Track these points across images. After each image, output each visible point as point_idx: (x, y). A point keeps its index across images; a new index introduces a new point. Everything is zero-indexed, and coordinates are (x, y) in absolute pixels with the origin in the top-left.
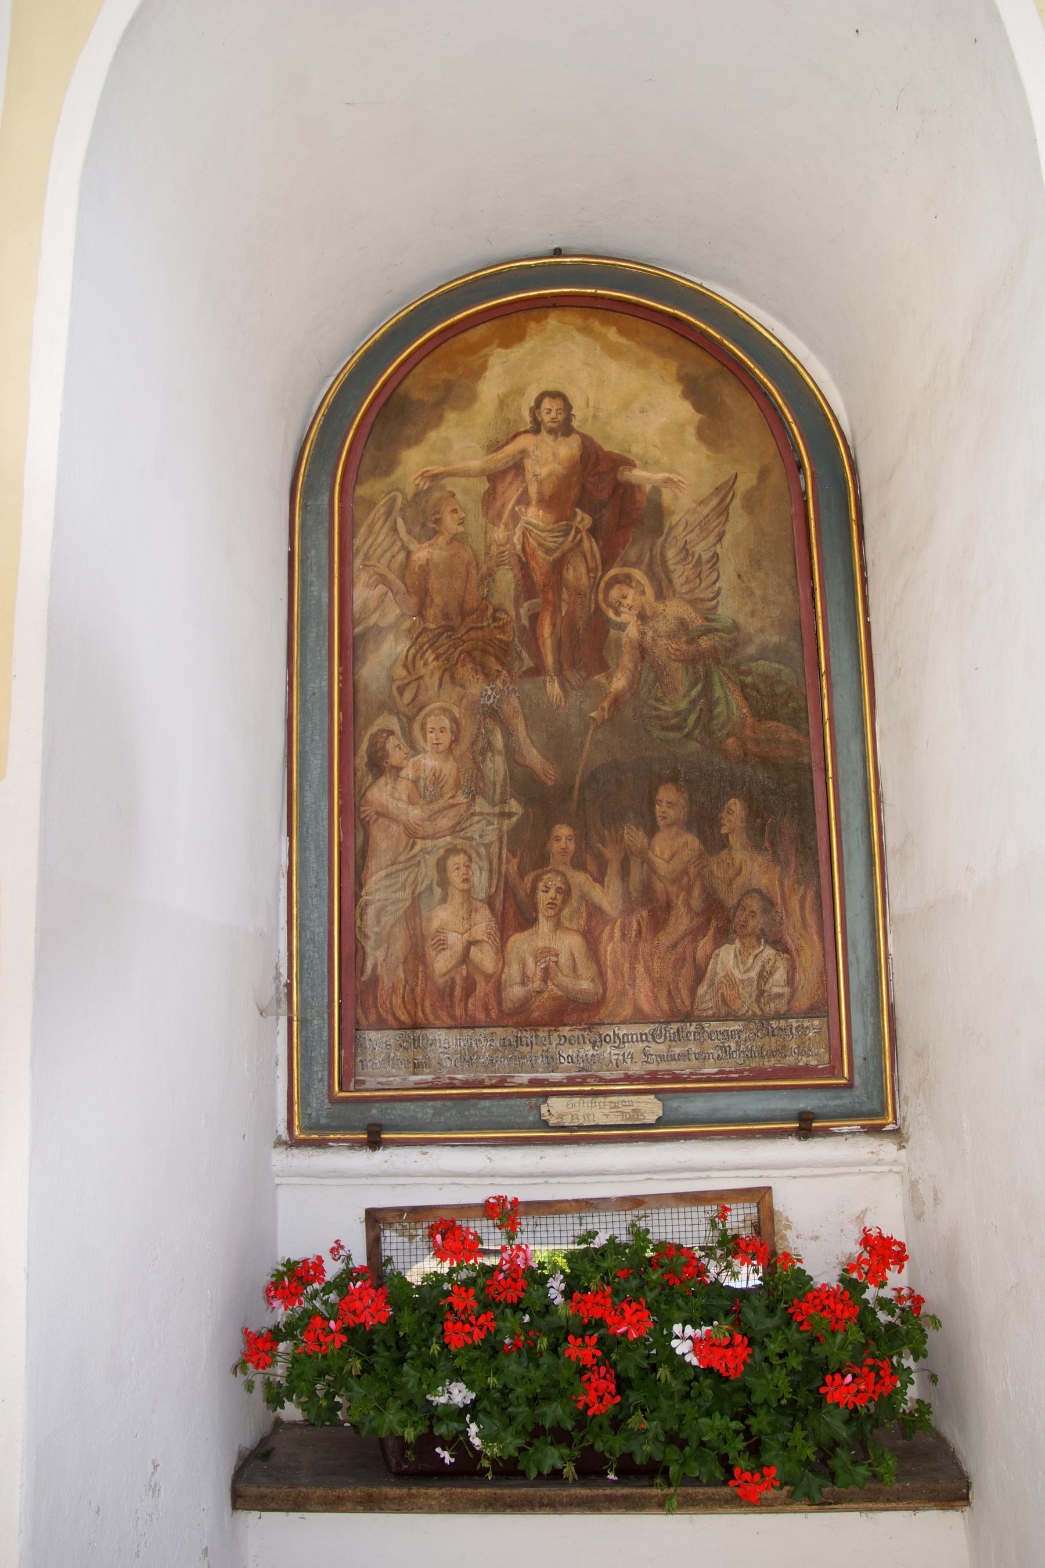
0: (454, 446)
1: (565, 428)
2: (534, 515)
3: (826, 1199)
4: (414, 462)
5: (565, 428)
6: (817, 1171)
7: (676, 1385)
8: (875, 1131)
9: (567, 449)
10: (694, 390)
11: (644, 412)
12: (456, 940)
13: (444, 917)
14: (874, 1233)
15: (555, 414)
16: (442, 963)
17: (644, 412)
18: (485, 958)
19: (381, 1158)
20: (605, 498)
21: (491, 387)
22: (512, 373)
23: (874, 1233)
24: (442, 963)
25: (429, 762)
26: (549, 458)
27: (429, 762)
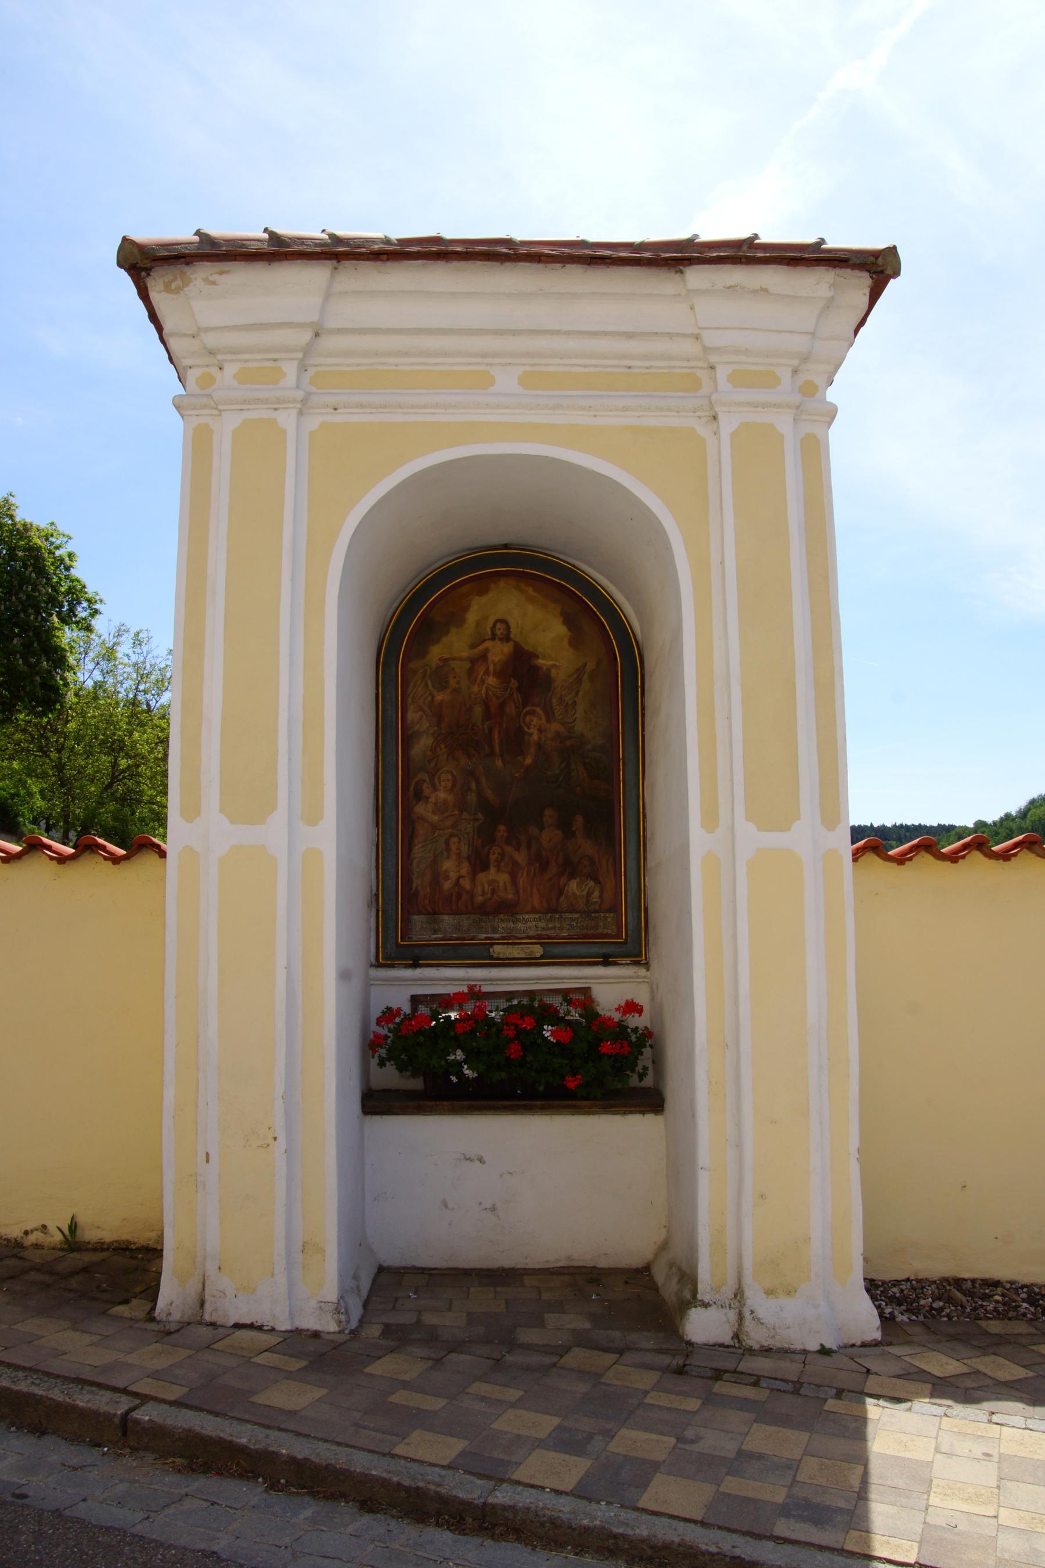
0: (454, 645)
1: (507, 638)
2: (491, 680)
3: (610, 987)
4: (436, 652)
5: (507, 638)
8: (637, 963)
9: (507, 648)
10: (569, 621)
11: (545, 632)
12: (453, 875)
13: (448, 865)
15: (502, 631)
16: (447, 885)
17: (545, 632)
18: (466, 884)
19: (418, 972)
20: (524, 671)
21: (472, 617)
24: (447, 885)
25: (442, 795)
26: (498, 652)
27: (442, 795)
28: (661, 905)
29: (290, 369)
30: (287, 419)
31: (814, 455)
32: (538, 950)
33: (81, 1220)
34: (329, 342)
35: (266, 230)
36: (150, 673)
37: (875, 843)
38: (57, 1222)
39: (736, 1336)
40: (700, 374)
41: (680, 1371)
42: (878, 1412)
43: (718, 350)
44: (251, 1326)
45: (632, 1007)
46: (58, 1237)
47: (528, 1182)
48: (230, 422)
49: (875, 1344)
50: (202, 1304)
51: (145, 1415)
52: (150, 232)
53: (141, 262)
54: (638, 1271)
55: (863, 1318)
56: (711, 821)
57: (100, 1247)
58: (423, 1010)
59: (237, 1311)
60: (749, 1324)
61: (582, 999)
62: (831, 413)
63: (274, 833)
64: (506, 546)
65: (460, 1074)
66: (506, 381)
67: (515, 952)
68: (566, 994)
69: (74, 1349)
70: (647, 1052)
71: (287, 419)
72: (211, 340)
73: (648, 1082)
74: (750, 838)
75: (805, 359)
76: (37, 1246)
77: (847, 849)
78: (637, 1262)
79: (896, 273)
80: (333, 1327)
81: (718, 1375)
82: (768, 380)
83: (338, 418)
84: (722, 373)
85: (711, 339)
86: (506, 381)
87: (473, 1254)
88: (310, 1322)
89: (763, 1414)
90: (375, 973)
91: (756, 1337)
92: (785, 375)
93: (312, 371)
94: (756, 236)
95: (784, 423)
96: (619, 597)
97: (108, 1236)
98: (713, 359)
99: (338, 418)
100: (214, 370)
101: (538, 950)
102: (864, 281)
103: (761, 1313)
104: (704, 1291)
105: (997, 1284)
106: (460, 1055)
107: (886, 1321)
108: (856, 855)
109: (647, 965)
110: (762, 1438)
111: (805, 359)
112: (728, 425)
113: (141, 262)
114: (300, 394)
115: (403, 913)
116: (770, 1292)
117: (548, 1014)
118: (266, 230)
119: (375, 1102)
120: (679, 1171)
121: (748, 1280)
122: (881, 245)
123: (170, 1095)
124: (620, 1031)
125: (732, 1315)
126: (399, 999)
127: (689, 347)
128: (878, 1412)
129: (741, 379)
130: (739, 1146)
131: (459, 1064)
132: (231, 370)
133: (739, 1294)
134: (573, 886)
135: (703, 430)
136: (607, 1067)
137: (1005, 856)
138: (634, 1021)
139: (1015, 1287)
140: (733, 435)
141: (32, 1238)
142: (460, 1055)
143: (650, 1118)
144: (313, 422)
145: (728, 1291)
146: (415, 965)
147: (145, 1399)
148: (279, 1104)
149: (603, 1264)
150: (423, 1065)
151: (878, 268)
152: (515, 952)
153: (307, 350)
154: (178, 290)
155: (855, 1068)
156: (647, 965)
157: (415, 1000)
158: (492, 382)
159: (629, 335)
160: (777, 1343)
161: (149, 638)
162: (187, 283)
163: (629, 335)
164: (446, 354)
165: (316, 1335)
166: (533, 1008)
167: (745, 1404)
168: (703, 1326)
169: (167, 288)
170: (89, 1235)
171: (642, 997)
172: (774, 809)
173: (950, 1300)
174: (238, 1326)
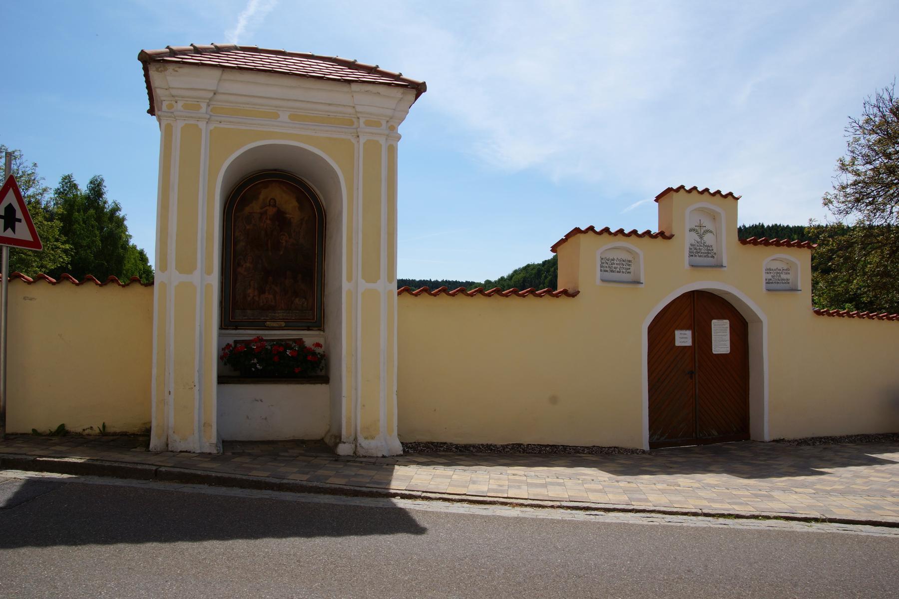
0: (255, 207)
1: (275, 206)
2: (268, 222)
3: (310, 338)
4: (247, 210)
5: (275, 206)
6: (511, 501)
7: (888, 151)
8: (320, 330)
9: (275, 210)
10: (298, 200)
11: (289, 204)
12: (251, 295)
13: (250, 291)
14: (121, 214)
15: (273, 203)
16: (249, 299)
17: (289, 204)
18: (257, 299)
19: (237, 331)
20: (281, 218)
21: (262, 197)
22: (264, 194)
23: (121, 214)
24: (249, 299)
25: (248, 265)
26: (271, 211)
27: (248, 265)
28: (330, 308)
29: (204, 106)
30: (202, 125)
31: (392, 152)
32: (283, 324)
33: (106, 424)
34: (218, 97)
35: (192, 45)
36: (21, 177)
37: (407, 287)
38: (97, 427)
39: (355, 453)
40: (354, 120)
41: (336, 460)
42: (396, 467)
43: (360, 112)
44: (186, 452)
45: (318, 345)
46: (98, 431)
47: (280, 408)
48: (179, 125)
49: (401, 455)
50: (167, 445)
51: (163, 469)
52: (152, 48)
53: (148, 60)
54: (319, 441)
55: (398, 448)
56: (350, 279)
57: (115, 434)
58: (239, 345)
59: (182, 446)
60: (359, 449)
61: (299, 342)
62: (399, 137)
63: (196, 277)
64: (275, 170)
65: (256, 368)
66: (284, 117)
67: (275, 324)
68: (295, 341)
69: (128, 458)
70: (323, 361)
71: (202, 125)
72: (174, 92)
73: (323, 373)
74: (363, 285)
75: (391, 118)
76: (89, 435)
77: (396, 291)
78: (319, 438)
79: (425, 91)
80: (215, 452)
81: (348, 461)
82: (378, 124)
83: (221, 126)
84: (362, 121)
85: (359, 109)
86: (284, 117)
87: (257, 436)
88: (207, 450)
89: (362, 468)
90: (224, 331)
91: (361, 452)
92: (384, 123)
93: (211, 107)
94: (377, 67)
95: (382, 141)
96: (318, 192)
97: (118, 430)
98: (359, 115)
99: (221, 126)
100: (173, 103)
101: (283, 324)
102: (414, 92)
103: (363, 445)
104: (344, 438)
105: (445, 443)
106: (255, 361)
107: (404, 451)
108: (399, 294)
109: (324, 331)
110: (362, 472)
111: (391, 118)
112: (363, 140)
113: (148, 60)
114: (208, 116)
115: (232, 310)
116: (366, 438)
117: (288, 346)
118: (192, 45)
119: (222, 379)
120: (335, 403)
121: (359, 434)
122: (420, 81)
123: (154, 371)
124: (314, 353)
125: (353, 446)
126: (231, 341)
127: (350, 110)
128: (396, 467)
129: (368, 123)
130: (356, 389)
131: (255, 364)
132: (180, 104)
133: (356, 439)
134: (297, 300)
135: (354, 141)
136: (310, 367)
137: (489, 295)
138: (319, 350)
139: (451, 444)
140: (365, 144)
141: (87, 432)
142: (255, 361)
143: (324, 385)
144: (212, 127)
145: (352, 438)
146: (236, 329)
147: (160, 466)
148: (197, 374)
149: (306, 439)
150: (240, 365)
151: (419, 89)
152: (275, 324)
153: (210, 100)
154: (161, 72)
155: (396, 363)
156: (324, 331)
157: (236, 342)
158: (278, 116)
159: (330, 105)
160: (368, 454)
161: (21, 156)
162: (166, 70)
163: (330, 105)
164: (262, 105)
165: (210, 454)
166: (283, 344)
167: (357, 466)
168: (344, 449)
169: (157, 70)
170: (110, 430)
171: (322, 342)
172: (372, 276)
173: (428, 448)
174: (181, 452)
